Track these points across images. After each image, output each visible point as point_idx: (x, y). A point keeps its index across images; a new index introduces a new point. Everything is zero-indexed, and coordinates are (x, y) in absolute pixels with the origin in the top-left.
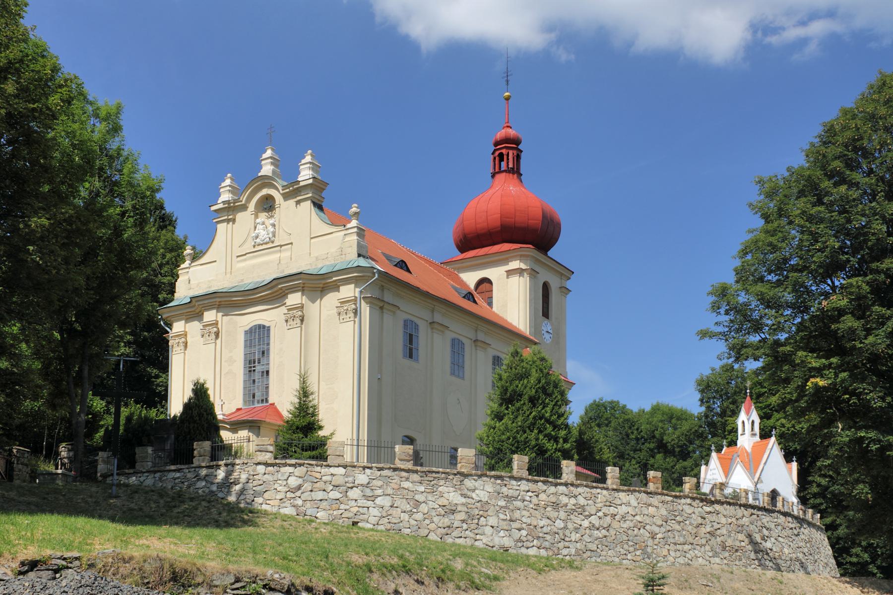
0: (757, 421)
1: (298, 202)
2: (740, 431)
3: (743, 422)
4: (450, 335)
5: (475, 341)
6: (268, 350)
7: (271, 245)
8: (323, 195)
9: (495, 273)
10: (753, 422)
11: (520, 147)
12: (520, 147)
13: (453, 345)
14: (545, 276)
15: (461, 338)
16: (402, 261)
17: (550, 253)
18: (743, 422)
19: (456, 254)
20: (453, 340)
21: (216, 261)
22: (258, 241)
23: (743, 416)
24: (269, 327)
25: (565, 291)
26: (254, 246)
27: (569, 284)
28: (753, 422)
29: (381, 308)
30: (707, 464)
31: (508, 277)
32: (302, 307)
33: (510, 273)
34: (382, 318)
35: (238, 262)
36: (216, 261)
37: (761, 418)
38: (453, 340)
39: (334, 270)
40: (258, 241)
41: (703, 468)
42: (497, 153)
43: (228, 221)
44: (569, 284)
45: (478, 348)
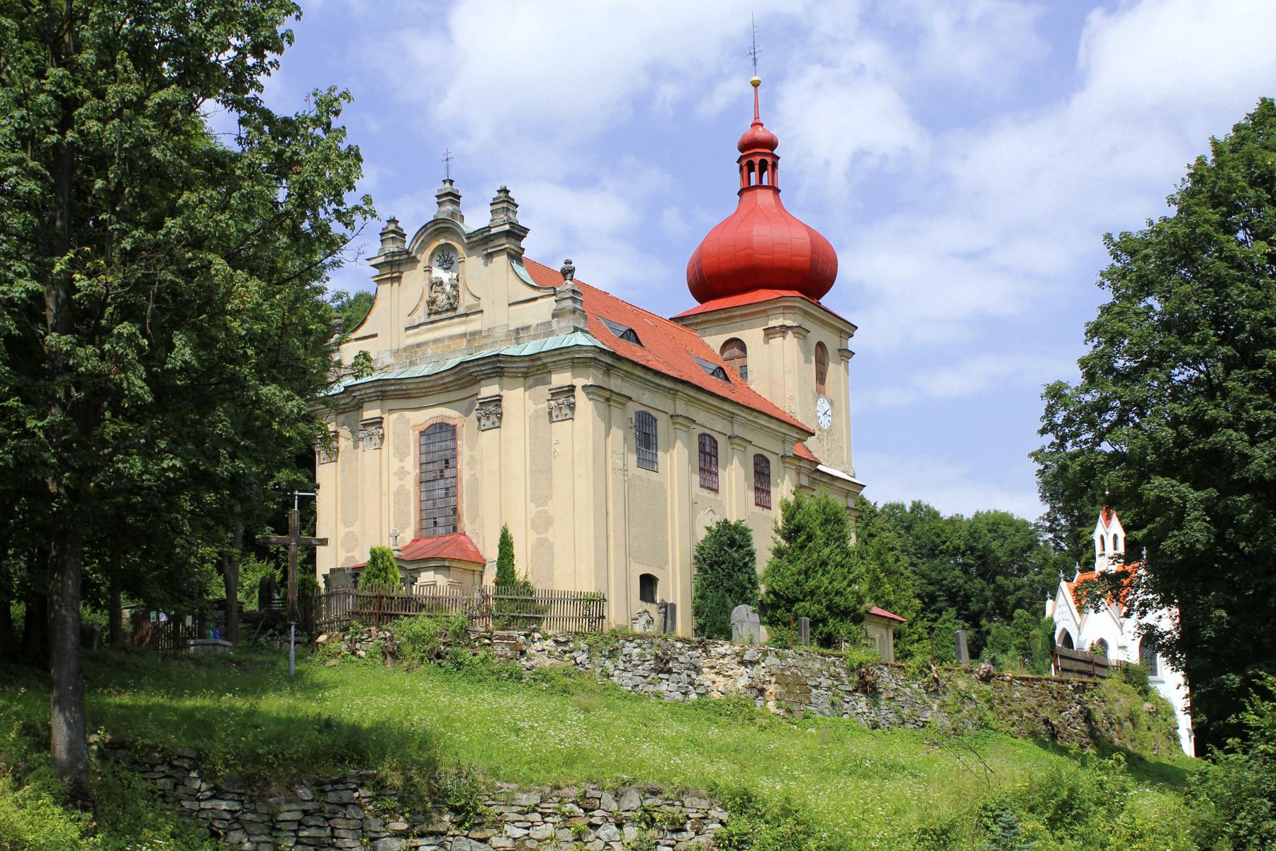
0: (1121, 535)
1: (489, 256)
2: (1098, 550)
3: (1102, 538)
4: (633, 408)
5: (782, 457)
6: (455, 457)
7: (450, 314)
8: (523, 244)
9: (752, 336)
10: (1115, 537)
11: (775, 152)
12: (775, 152)
13: (702, 445)
14: (818, 334)
15: (715, 435)
16: (631, 330)
17: (825, 301)
18: (1102, 538)
19: (690, 304)
20: (756, 456)
21: (375, 336)
22: (434, 308)
23: (1100, 529)
24: (455, 426)
25: (846, 354)
26: (429, 315)
27: (852, 344)
28: (1115, 537)
29: (608, 400)
30: (1054, 597)
31: (766, 342)
32: (500, 401)
33: (769, 333)
34: (610, 412)
35: (408, 336)
36: (375, 336)
37: (1127, 529)
38: (756, 456)
39: (543, 350)
40: (434, 308)
41: (1049, 603)
42: (744, 162)
43: (392, 280)
44: (852, 344)
45: (612, 403)
